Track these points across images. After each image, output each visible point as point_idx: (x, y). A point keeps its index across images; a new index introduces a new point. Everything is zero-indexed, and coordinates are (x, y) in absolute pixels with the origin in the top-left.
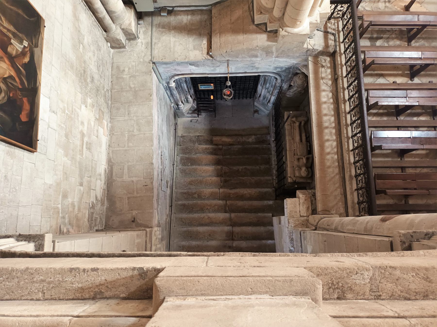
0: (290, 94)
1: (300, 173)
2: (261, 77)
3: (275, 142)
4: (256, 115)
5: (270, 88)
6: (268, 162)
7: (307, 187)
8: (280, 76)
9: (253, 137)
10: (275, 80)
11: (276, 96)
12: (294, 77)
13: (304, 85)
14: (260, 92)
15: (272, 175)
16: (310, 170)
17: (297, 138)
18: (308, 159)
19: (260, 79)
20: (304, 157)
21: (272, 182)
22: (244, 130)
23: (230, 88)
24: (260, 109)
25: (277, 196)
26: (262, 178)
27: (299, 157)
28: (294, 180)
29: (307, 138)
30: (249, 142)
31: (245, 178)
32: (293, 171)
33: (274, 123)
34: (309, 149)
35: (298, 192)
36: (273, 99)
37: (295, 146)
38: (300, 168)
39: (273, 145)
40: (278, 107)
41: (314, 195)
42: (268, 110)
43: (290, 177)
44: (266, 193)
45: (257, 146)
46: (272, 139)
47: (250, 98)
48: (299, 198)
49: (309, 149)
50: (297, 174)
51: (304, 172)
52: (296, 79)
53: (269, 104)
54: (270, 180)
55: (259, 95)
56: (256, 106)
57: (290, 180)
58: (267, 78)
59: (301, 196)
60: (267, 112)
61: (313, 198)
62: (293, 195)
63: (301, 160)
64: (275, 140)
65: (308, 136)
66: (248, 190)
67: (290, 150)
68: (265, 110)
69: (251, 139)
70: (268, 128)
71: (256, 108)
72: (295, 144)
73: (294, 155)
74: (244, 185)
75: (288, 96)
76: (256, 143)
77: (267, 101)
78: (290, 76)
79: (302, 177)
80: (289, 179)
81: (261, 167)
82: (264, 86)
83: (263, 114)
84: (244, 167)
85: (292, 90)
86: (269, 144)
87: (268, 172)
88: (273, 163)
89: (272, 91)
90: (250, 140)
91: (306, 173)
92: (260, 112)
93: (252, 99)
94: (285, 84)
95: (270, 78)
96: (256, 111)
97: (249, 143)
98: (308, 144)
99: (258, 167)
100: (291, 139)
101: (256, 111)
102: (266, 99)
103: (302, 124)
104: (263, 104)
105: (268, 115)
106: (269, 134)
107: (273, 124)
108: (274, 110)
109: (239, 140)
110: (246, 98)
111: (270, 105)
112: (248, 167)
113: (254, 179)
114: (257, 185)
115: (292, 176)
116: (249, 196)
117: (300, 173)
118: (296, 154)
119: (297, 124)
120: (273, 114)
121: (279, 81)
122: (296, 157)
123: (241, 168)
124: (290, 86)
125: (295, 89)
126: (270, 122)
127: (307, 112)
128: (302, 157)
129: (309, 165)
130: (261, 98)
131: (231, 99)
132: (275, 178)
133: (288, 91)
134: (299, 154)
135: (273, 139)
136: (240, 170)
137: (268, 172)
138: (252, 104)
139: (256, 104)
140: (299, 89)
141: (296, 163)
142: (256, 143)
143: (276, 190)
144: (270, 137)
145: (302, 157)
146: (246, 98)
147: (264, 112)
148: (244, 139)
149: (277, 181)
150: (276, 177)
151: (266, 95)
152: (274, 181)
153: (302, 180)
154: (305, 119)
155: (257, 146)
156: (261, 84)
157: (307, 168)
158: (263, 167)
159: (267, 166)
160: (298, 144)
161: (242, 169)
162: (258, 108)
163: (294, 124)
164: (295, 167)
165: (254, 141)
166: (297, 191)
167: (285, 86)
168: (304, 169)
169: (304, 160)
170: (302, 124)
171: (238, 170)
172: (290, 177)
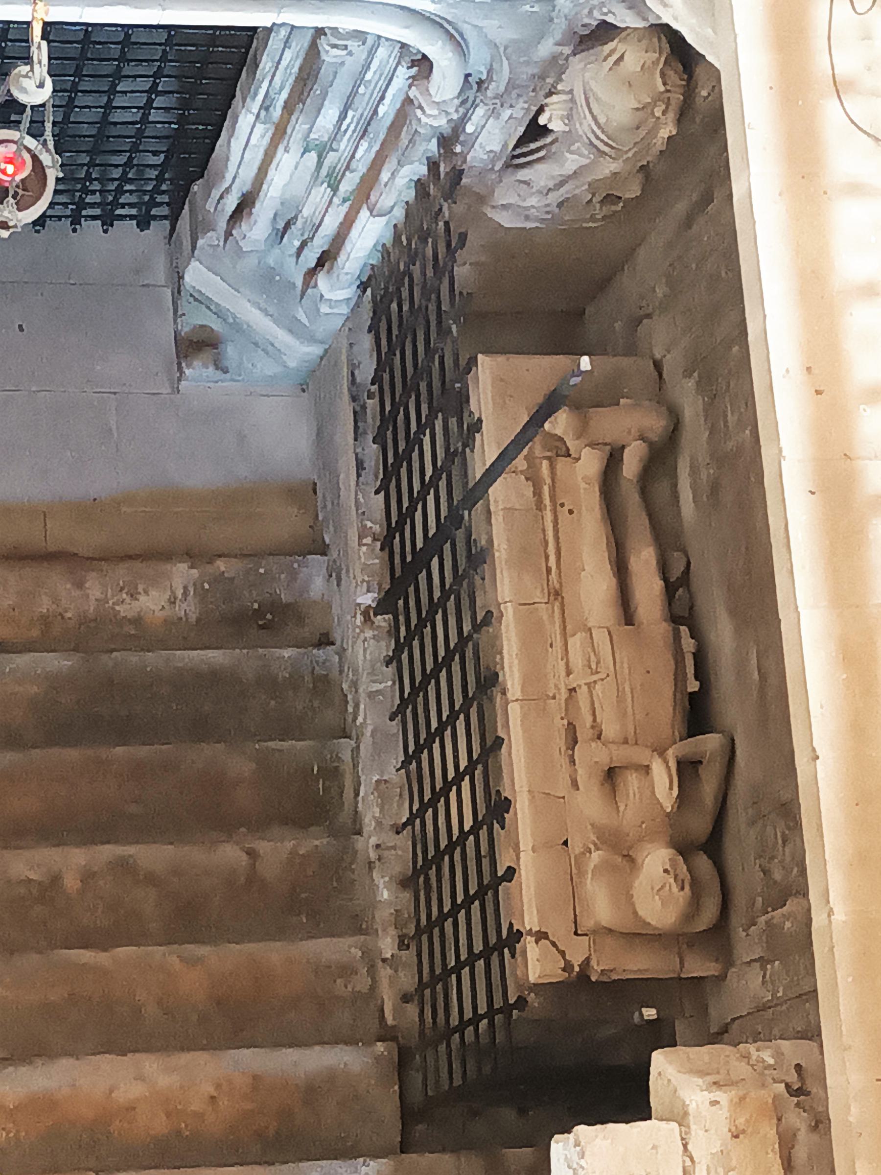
0: (523, 202)
1: (624, 896)
2: (275, 43)
3: (382, 621)
4: (198, 372)
5: (344, 145)
6: (316, 802)
7: (680, 1027)
8: (458, 42)
9: (182, 574)
10: (403, 73)
11: (399, 214)
12: (576, 63)
13: (653, 132)
14: (248, 174)
15: (359, 924)
16: (703, 862)
17: (594, 587)
18: (688, 770)
19: (266, 64)
20: (661, 753)
21: (362, 983)
22: (87, 511)
23: (36, 132)
24: (237, 327)
25: (408, 1115)
26: (274, 953)
27: (620, 755)
28: (577, 961)
29: (670, 589)
30: (137, 621)
31: (124, 952)
32: (579, 885)
33: (372, 449)
34: (693, 686)
35: (663, 1066)
36: (368, 237)
37: (577, 659)
38: (623, 853)
39: (365, 651)
40: (428, 315)
41: (804, 1089)
42: (312, 339)
43: (541, 936)
44: (312, 1091)
45: (216, 657)
46: (351, 587)
47: (143, 223)
48: (681, 1118)
49: (693, 686)
50: (602, 908)
51: (657, 890)
52: (588, 75)
53: (322, 280)
54: (346, 971)
55: (231, 203)
56: (200, 299)
57: (536, 965)
58: (330, 55)
59: (696, 1096)
60: (299, 352)
61: (797, 1120)
62: (625, 1097)
63: (632, 781)
64: (385, 605)
65: (676, 571)
66: (150, 1064)
67: (536, 699)
68: (281, 336)
69: (163, 596)
70: (304, 494)
71: (195, 318)
72: (576, 643)
73: (573, 741)
74: (118, 1031)
75: (506, 220)
76: (200, 633)
77: (311, 257)
78: (546, 49)
79: (640, 936)
80: (532, 949)
81: (263, 846)
82: (298, 128)
83: (265, 367)
84: (108, 852)
85: (541, 174)
86: (325, 640)
87: (320, 900)
88: (370, 813)
89: (361, 166)
90: (152, 603)
91: (682, 897)
92: (231, 351)
93: (159, 228)
94: (494, 113)
95: (360, 52)
96: (198, 345)
97: (140, 635)
98: (688, 644)
99: (230, 854)
100: (538, 596)
101: (198, 345)
102: (293, 241)
103: (631, 465)
104: (268, 282)
105: (311, 382)
106: (323, 550)
107: (360, 466)
108: (366, 341)
109: (45, 605)
110: (108, 220)
111: (338, 291)
112: (153, 856)
113: (195, 969)
114: (235, 1020)
115: (560, 931)
116: (160, 1125)
117: (624, 896)
118: (584, 732)
119: (589, 464)
120: (367, 370)
121: (446, 82)
122: (592, 756)
123: (72, 861)
124: (535, 130)
125: (571, 162)
126: (322, 439)
127: (658, 366)
128: (641, 755)
129: (700, 825)
130: (257, 229)
131: (40, 222)
132: (387, 945)
133: (510, 178)
134: (610, 730)
135: (368, 599)
136: (71, 883)
137: (320, 900)
138: (160, 273)
139: (196, 275)
140: (608, 167)
141: (589, 803)
142: (200, 633)
143: (403, 1061)
144: (335, 574)
145: (641, 755)
146: (108, 220)
147: (269, 349)
148: (96, 592)
149: (408, 980)
150: (402, 945)
151: (302, 205)
152: (385, 973)
153: (638, 964)
154: (655, 423)
155: (216, 657)
156: (266, 107)
157: (684, 849)
158: (277, 850)
159: (316, 842)
160: (601, 638)
161: (88, 876)
162: (219, 314)
163: (562, 463)
164: (576, 847)
165: (189, 609)
166: (659, 1059)
167: (491, 135)
168: (656, 860)
169: (663, 784)
170: (631, 465)
171: (56, 880)
172: (541, 936)
